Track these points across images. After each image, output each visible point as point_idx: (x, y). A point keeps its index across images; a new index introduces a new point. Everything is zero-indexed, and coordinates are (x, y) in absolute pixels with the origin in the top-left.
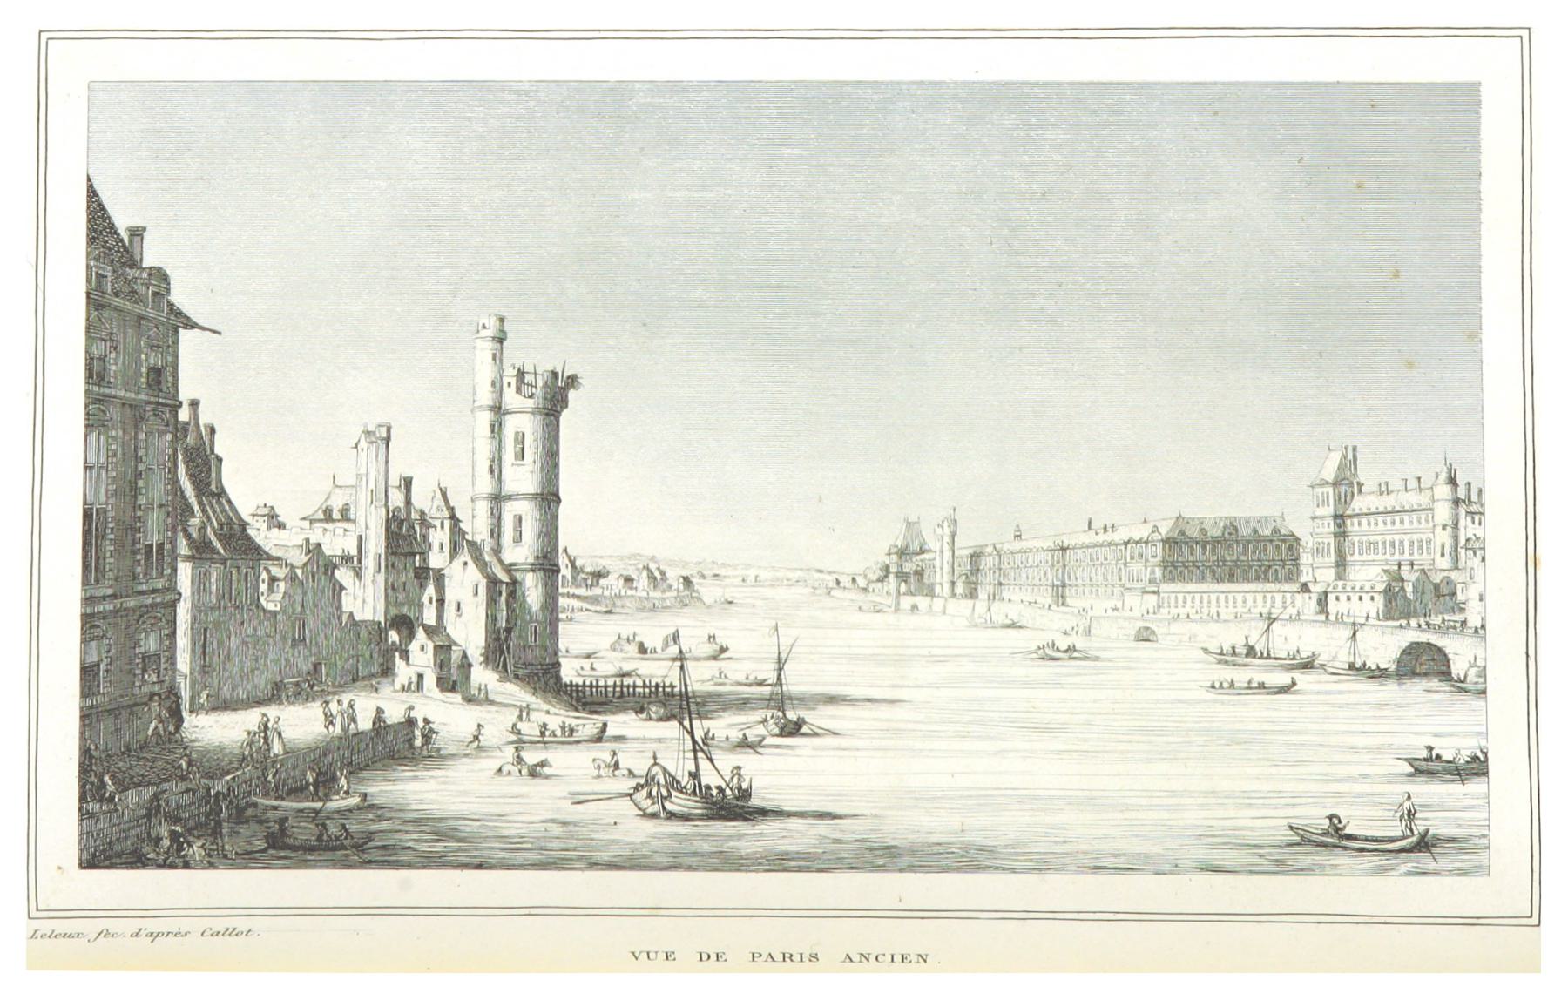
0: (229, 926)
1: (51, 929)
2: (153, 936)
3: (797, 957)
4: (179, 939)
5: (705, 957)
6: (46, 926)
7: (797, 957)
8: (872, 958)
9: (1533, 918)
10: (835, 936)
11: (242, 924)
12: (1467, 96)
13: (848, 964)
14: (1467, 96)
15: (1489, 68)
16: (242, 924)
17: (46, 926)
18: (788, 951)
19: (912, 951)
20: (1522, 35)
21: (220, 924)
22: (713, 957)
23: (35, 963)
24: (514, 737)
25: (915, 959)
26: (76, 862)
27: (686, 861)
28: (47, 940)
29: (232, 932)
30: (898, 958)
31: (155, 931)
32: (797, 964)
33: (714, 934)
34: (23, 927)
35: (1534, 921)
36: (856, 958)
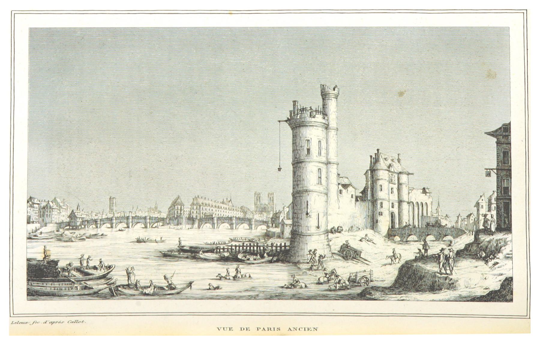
0: (76, 318)
1: (17, 320)
2: (52, 323)
3: (272, 329)
4: (60, 324)
5: (242, 329)
6: (16, 320)
7: (272, 329)
8: (298, 329)
9: (528, 316)
10: (284, 322)
11: (80, 319)
12: (33, 32)
13: (290, 331)
14: (33, 32)
15: (24, 25)
16: (80, 319)
17: (16, 320)
18: (269, 327)
19: (312, 326)
20: (13, 14)
21: (74, 319)
22: (245, 329)
23: (11, 334)
24: (197, 196)
25: (313, 329)
26: (511, 33)
27: (215, 297)
28: (16, 324)
29: (77, 322)
30: (306, 329)
31: (52, 320)
32: (273, 332)
33: (244, 321)
34: (7, 320)
35: (528, 317)
36: (292, 329)
